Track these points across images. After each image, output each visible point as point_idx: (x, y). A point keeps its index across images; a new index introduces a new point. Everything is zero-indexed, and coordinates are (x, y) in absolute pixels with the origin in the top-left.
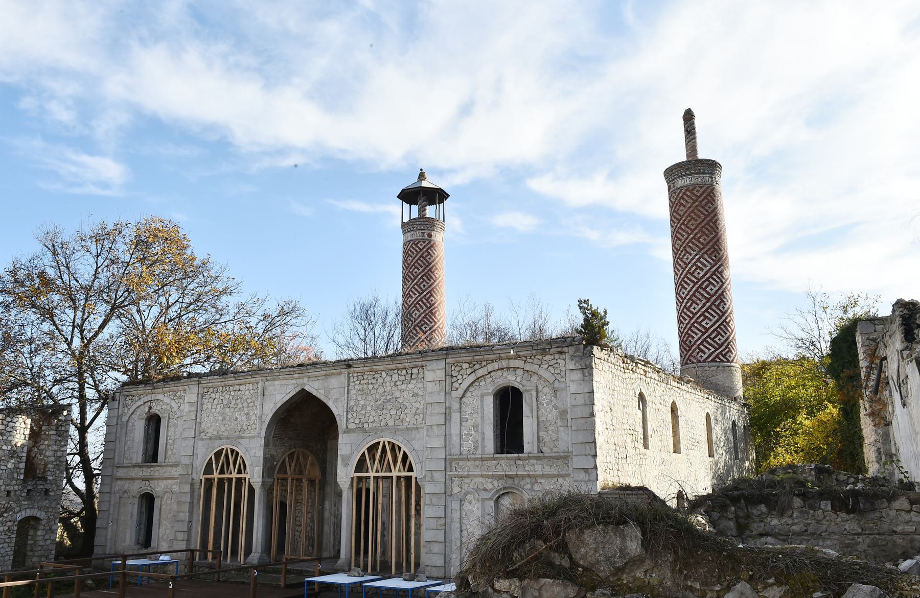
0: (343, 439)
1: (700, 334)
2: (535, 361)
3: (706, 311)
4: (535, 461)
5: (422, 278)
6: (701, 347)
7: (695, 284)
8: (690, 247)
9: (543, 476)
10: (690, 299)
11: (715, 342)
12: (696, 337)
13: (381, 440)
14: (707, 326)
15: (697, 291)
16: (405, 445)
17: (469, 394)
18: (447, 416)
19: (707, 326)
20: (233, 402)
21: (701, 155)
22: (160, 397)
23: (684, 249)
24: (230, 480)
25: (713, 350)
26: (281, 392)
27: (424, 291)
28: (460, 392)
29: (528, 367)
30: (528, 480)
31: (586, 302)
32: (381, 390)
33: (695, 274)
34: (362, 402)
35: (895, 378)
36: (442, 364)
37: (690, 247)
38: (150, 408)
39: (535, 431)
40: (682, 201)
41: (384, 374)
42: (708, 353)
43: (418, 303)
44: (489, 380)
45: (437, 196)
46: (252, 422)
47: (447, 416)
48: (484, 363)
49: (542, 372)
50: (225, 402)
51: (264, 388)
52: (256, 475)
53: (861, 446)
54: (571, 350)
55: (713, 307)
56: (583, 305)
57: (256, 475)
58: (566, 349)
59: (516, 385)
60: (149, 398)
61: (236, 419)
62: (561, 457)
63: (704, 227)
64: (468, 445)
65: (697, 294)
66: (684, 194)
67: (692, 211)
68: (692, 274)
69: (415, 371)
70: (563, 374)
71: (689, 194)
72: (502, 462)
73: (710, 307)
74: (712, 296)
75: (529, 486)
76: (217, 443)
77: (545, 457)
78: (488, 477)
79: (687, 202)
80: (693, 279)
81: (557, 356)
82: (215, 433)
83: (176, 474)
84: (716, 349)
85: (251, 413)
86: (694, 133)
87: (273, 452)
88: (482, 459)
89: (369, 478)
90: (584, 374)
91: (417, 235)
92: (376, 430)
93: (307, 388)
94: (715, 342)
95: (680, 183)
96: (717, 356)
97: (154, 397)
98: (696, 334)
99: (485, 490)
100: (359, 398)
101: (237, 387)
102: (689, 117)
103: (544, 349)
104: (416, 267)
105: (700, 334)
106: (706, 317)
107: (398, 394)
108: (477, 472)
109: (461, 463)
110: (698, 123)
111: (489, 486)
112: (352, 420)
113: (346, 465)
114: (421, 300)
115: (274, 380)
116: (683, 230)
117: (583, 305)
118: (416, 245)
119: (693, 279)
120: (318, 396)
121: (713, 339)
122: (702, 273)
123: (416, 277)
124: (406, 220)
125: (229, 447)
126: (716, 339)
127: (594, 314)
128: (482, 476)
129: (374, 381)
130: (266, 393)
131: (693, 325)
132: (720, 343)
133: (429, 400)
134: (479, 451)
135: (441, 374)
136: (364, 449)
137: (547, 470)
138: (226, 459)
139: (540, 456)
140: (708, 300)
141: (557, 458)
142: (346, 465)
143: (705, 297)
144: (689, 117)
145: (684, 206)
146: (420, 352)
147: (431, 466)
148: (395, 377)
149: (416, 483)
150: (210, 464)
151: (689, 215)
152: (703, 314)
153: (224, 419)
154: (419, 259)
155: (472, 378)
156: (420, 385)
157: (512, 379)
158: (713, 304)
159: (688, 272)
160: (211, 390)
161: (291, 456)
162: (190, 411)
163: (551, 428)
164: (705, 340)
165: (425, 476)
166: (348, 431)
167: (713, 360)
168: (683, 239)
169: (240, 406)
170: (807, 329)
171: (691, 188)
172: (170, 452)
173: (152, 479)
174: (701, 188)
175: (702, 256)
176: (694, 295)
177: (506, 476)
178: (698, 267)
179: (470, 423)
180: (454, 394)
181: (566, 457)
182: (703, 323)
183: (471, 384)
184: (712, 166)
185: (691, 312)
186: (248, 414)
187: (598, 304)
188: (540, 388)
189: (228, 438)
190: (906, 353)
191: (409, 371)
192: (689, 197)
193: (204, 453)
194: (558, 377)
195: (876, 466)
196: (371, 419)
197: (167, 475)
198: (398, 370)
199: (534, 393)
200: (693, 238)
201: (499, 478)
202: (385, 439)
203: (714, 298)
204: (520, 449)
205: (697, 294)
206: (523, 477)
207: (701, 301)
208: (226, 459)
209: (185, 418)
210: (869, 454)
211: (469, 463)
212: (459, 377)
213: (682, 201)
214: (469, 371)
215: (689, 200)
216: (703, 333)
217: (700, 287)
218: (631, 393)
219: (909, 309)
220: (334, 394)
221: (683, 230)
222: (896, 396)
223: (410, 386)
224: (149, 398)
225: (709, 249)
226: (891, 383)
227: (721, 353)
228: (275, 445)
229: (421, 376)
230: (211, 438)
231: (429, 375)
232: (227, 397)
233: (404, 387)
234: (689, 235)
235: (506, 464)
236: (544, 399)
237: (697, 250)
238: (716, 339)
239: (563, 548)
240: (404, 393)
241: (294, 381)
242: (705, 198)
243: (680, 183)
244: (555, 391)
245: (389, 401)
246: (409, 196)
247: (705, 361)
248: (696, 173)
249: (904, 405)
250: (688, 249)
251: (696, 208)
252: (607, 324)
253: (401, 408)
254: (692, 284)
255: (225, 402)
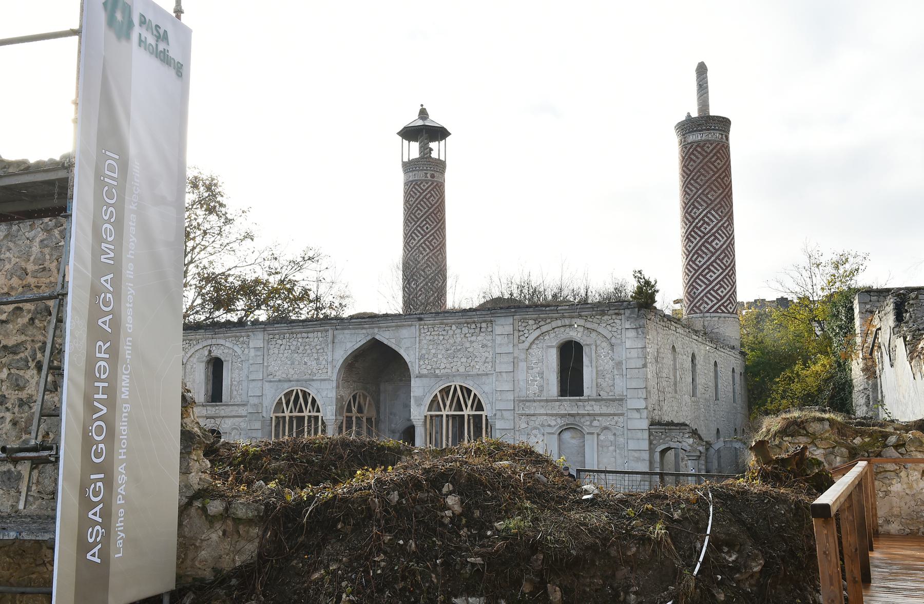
0: (414, 383)
1: (704, 286)
2: (595, 320)
3: (711, 264)
4: (593, 403)
5: (425, 220)
6: (705, 299)
7: (702, 238)
8: (698, 202)
9: (601, 415)
10: (696, 252)
11: (718, 294)
12: (700, 289)
13: (453, 384)
14: (711, 279)
15: (703, 245)
16: (476, 389)
17: (534, 346)
18: (514, 364)
19: (711, 279)
20: (302, 348)
21: (713, 112)
22: (222, 342)
23: (693, 204)
24: (284, 417)
25: (715, 301)
26: (352, 342)
27: (427, 234)
28: (527, 344)
29: (588, 325)
30: (587, 418)
31: (640, 272)
32: (451, 341)
33: (702, 229)
34: (433, 351)
35: (887, 345)
36: (510, 320)
37: (698, 202)
38: (210, 351)
39: (594, 379)
40: (692, 156)
41: (454, 327)
42: (711, 304)
43: (421, 245)
44: (552, 335)
45: (440, 133)
46: (322, 367)
47: (514, 364)
48: (549, 321)
49: (600, 330)
50: (293, 348)
51: (334, 337)
52: (329, 414)
53: (851, 393)
54: (628, 312)
55: (718, 261)
56: (638, 275)
57: (329, 414)
58: (622, 312)
59: (578, 340)
60: (209, 342)
61: (306, 364)
62: (617, 400)
63: (712, 183)
64: (535, 388)
65: (703, 248)
66: (695, 149)
67: (702, 167)
68: (699, 229)
69: (484, 325)
70: (619, 332)
71: (699, 149)
72: (564, 403)
73: (714, 261)
74: (717, 250)
75: (588, 423)
76: (286, 385)
77: (602, 400)
78: (552, 415)
79: (698, 158)
80: (700, 233)
81: (614, 317)
82: (284, 376)
83: (244, 413)
84: (719, 301)
85: (321, 358)
86: (707, 87)
87: (342, 393)
88: (547, 401)
89: (442, 416)
90: (638, 333)
91: (420, 176)
92: (447, 376)
93: (377, 337)
94: (718, 294)
95: (692, 138)
96: (719, 307)
97: (214, 341)
98: (701, 286)
99: (549, 426)
100: (431, 347)
101: (305, 335)
102: (702, 70)
103: (603, 311)
104: (419, 209)
105: (704, 286)
106: (710, 271)
107: (468, 345)
108: (542, 411)
109: (527, 404)
110: (710, 74)
111: (553, 423)
112: (424, 366)
113: (419, 405)
114: (424, 242)
115: (343, 329)
116: (692, 185)
117: (638, 275)
118: (419, 186)
119: (700, 233)
120: (389, 344)
121: (716, 292)
122: (709, 228)
123: (419, 220)
124: (406, 160)
125: (299, 388)
126: (719, 292)
127: (647, 283)
128: (547, 415)
129: (444, 333)
130: (336, 341)
131: (698, 277)
132: (722, 295)
133: (498, 351)
134: (545, 393)
135: (509, 329)
136: (437, 392)
137: (604, 410)
138: (298, 399)
139: (598, 400)
140: (713, 254)
141: (613, 400)
142: (419, 405)
143: (711, 251)
144: (702, 70)
145: (695, 162)
146: (489, 309)
147: (500, 406)
148: (465, 330)
149: (487, 420)
150: (280, 403)
151: (699, 171)
152: (708, 267)
153: (293, 363)
154: (422, 200)
155: (538, 333)
156: (489, 337)
157: (576, 335)
158: (717, 258)
159: (695, 226)
160: (277, 336)
161: (354, 397)
162: (256, 356)
163: (608, 376)
164: (708, 292)
165: (495, 415)
166: (420, 376)
167: (716, 311)
168: (692, 194)
169: (309, 351)
170: (801, 282)
171: (702, 144)
172: (235, 393)
173: (217, 417)
174: (711, 144)
175: (709, 212)
176: (700, 248)
177: (569, 414)
178: (705, 222)
179: (536, 370)
180: (521, 346)
181: (622, 400)
182: (708, 276)
183: (537, 338)
184: (723, 124)
185: (697, 265)
186: (318, 359)
187: (649, 275)
188: (598, 342)
189: (298, 381)
190: (896, 330)
191: (478, 325)
192: (699, 153)
193: (272, 395)
194: (615, 334)
195: (865, 408)
196: (443, 366)
197: (234, 414)
198: (468, 323)
199: (594, 347)
200: (702, 193)
201: (562, 416)
202: (458, 382)
203: (719, 252)
204: (581, 393)
205: (703, 248)
206: (583, 415)
207: (706, 254)
208: (298, 399)
209: (251, 362)
210: (858, 399)
211: (535, 404)
212: (526, 331)
213: (692, 156)
214: (535, 327)
215: (699, 156)
216: (707, 286)
217: (706, 241)
218: (668, 347)
219: (901, 298)
220: (406, 343)
221: (692, 185)
222: (886, 358)
223: (479, 338)
224: (209, 342)
225: (716, 205)
226: (883, 347)
227: (722, 304)
228: (343, 388)
229: (490, 329)
230: (280, 381)
231: (498, 330)
232: (295, 343)
233: (474, 338)
234: (698, 190)
235: (568, 405)
236: (602, 352)
237: (705, 205)
238: (719, 292)
239: (804, 428)
240: (475, 344)
241: (364, 331)
242: (715, 154)
243: (692, 138)
244: (612, 345)
245: (459, 350)
246: (409, 133)
247: (708, 312)
248: (708, 130)
249: (892, 366)
250: (696, 204)
251: (706, 164)
252: (657, 291)
253: (471, 356)
254: (698, 238)
255: (293, 348)
